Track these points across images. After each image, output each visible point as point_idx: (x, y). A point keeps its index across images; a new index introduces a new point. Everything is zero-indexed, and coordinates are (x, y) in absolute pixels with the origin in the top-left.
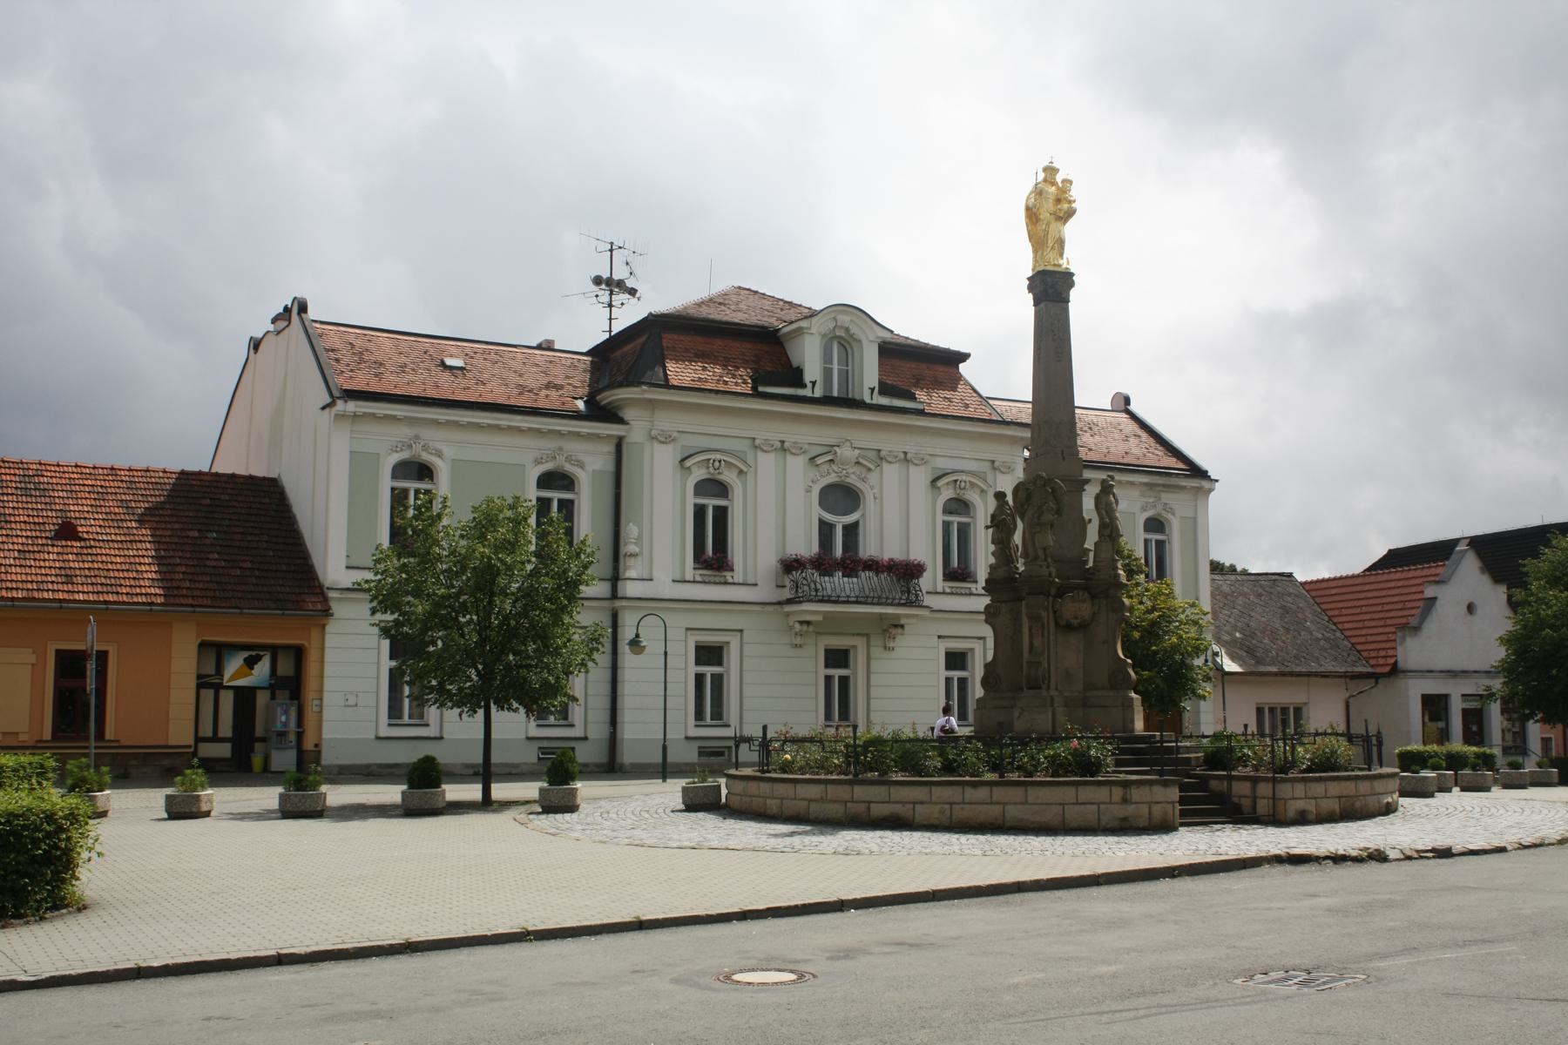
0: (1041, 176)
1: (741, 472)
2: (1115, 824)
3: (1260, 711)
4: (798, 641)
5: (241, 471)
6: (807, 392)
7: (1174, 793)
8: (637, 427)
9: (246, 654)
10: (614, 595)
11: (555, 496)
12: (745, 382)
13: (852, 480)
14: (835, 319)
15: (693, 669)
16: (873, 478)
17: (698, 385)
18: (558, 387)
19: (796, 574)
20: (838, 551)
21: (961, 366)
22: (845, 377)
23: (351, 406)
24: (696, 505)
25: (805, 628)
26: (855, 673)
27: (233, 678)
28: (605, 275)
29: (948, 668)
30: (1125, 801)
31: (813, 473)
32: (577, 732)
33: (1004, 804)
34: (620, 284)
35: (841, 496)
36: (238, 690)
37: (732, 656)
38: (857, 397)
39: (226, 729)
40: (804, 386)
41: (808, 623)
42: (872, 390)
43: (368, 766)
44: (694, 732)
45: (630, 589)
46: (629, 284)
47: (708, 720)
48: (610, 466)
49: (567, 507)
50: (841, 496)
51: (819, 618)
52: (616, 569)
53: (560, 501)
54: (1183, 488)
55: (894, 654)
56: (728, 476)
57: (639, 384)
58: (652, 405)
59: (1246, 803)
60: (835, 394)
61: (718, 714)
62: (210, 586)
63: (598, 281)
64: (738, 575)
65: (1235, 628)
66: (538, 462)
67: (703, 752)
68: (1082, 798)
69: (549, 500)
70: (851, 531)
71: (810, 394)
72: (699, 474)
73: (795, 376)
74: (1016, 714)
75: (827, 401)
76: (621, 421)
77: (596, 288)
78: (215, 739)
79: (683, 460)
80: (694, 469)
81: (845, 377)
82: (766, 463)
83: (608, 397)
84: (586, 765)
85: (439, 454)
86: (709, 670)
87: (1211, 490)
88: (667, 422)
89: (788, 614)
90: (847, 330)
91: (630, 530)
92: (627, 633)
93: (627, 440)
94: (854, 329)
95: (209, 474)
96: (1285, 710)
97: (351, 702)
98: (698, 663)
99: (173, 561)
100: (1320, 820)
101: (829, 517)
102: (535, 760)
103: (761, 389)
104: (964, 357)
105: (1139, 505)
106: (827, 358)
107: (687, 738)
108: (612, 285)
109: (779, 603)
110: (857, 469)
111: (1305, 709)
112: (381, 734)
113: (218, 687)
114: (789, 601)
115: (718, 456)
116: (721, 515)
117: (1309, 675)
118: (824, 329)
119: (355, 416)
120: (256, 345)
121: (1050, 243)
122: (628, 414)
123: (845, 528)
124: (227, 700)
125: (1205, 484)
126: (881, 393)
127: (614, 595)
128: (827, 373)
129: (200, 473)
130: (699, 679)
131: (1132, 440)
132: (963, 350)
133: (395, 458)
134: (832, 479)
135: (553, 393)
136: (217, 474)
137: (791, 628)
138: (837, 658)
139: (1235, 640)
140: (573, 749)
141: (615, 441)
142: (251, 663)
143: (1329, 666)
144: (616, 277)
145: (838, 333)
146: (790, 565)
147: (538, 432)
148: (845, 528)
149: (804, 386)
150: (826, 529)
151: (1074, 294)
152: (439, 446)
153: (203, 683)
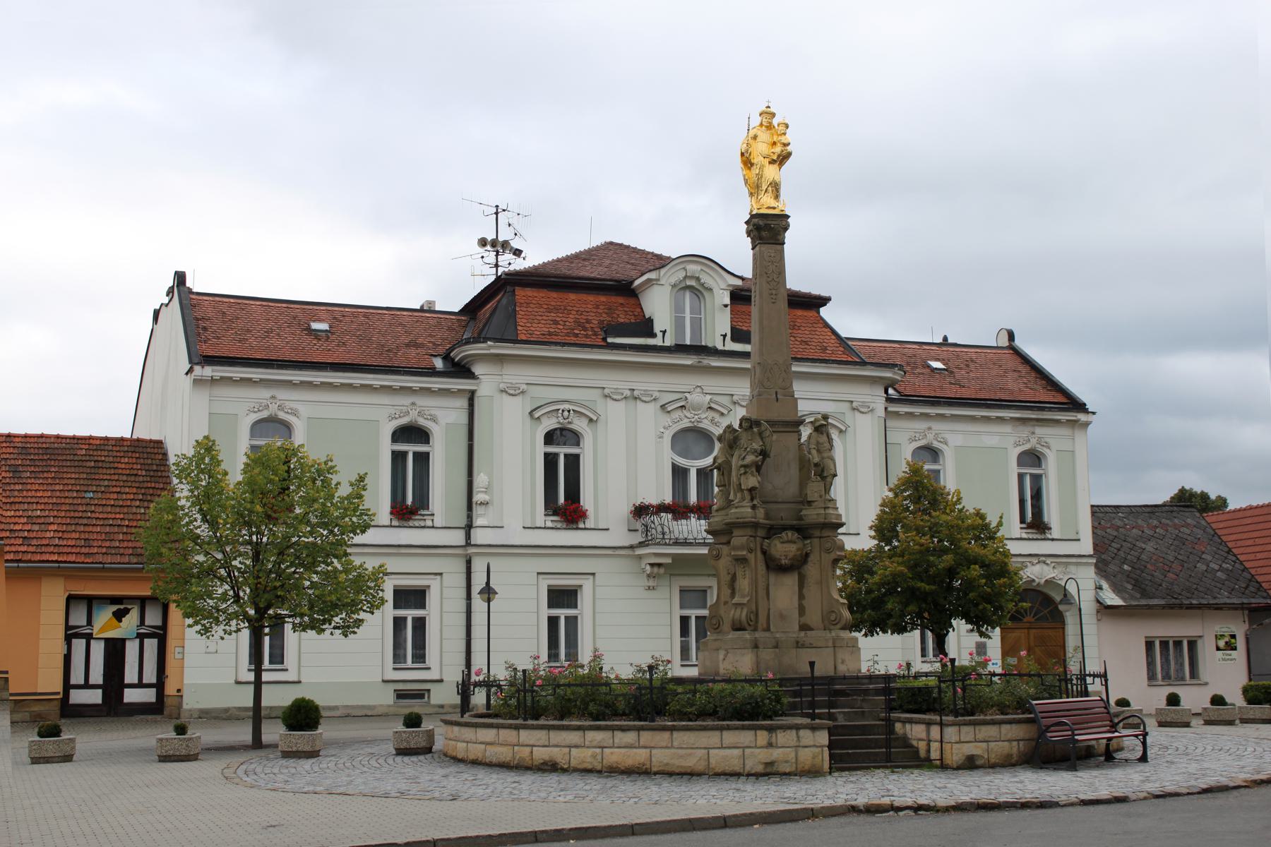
0: (756, 120)
1: (591, 420)
2: (760, 769)
3: (1149, 645)
5: (147, 437)
6: (657, 341)
7: (823, 738)
8: (487, 380)
9: (115, 608)
10: (468, 543)
11: (411, 448)
12: (595, 334)
17: (547, 339)
18: (417, 346)
19: (647, 519)
20: (693, 498)
21: (822, 310)
22: (697, 325)
23: (208, 371)
24: (546, 455)
25: (656, 569)
27: (102, 630)
28: (490, 236)
30: (770, 745)
31: (666, 420)
32: (433, 675)
33: (603, 748)
34: (505, 245)
36: (108, 641)
37: (585, 599)
38: (710, 345)
39: (97, 676)
40: (653, 335)
41: (659, 565)
42: (724, 336)
43: (227, 710)
45: (479, 536)
46: (515, 244)
48: (464, 419)
49: (423, 460)
51: (669, 561)
52: (470, 517)
53: (415, 454)
54: (1058, 422)
56: (579, 425)
57: (485, 340)
58: (500, 359)
59: (922, 746)
60: (688, 342)
61: (420, 656)
62: (78, 543)
63: (483, 243)
65: (1124, 561)
66: (392, 418)
67: (401, 695)
68: (726, 742)
69: (404, 454)
71: (660, 343)
72: (550, 424)
73: (646, 327)
74: (721, 657)
75: (680, 349)
76: (471, 375)
77: (481, 250)
78: (87, 685)
79: (531, 413)
81: (697, 325)
82: (614, 413)
83: (458, 354)
84: (442, 706)
85: (295, 413)
87: (1087, 424)
88: (516, 375)
89: (640, 557)
90: (698, 279)
91: (480, 479)
92: (479, 582)
93: (477, 394)
94: (705, 279)
95: (131, 440)
96: (1178, 644)
98: (550, 606)
99: (47, 520)
100: (992, 766)
101: (682, 462)
102: (392, 703)
103: (610, 340)
104: (823, 301)
105: (1012, 440)
106: (678, 308)
108: (498, 246)
109: (632, 547)
110: (711, 414)
111: (1200, 643)
112: (386, 678)
113: (89, 637)
114: (641, 545)
115: (567, 406)
116: (573, 463)
117: (1200, 607)
118: (673, 280)
119: (213, 381)
120: (156, 314)
121: (764, 188)
122: (478, 369)
123: (700, 472)
124: (98, 650)
125: (1082, 417)
126: (734, 339)
127: (468, 543)
128: (679, 323)
129: (122, 439)
130: (553, 622)
131: (1010, 375)
132: (824, 294)
134: (685, 424)
135: (413, 352)
136: (138, 440)
137: (644, 571)
139: (1122, 571)
140: (429, 691)
141: (468, 395)
142: (119, 616)
143: (1224, 598)
144: (501, 239)
145: (689, 283)
146: (640, 511)
149: (653, 335)
150: (679, 474)
151: (788, 235)
152: (293, 405)
153: (71, 635)
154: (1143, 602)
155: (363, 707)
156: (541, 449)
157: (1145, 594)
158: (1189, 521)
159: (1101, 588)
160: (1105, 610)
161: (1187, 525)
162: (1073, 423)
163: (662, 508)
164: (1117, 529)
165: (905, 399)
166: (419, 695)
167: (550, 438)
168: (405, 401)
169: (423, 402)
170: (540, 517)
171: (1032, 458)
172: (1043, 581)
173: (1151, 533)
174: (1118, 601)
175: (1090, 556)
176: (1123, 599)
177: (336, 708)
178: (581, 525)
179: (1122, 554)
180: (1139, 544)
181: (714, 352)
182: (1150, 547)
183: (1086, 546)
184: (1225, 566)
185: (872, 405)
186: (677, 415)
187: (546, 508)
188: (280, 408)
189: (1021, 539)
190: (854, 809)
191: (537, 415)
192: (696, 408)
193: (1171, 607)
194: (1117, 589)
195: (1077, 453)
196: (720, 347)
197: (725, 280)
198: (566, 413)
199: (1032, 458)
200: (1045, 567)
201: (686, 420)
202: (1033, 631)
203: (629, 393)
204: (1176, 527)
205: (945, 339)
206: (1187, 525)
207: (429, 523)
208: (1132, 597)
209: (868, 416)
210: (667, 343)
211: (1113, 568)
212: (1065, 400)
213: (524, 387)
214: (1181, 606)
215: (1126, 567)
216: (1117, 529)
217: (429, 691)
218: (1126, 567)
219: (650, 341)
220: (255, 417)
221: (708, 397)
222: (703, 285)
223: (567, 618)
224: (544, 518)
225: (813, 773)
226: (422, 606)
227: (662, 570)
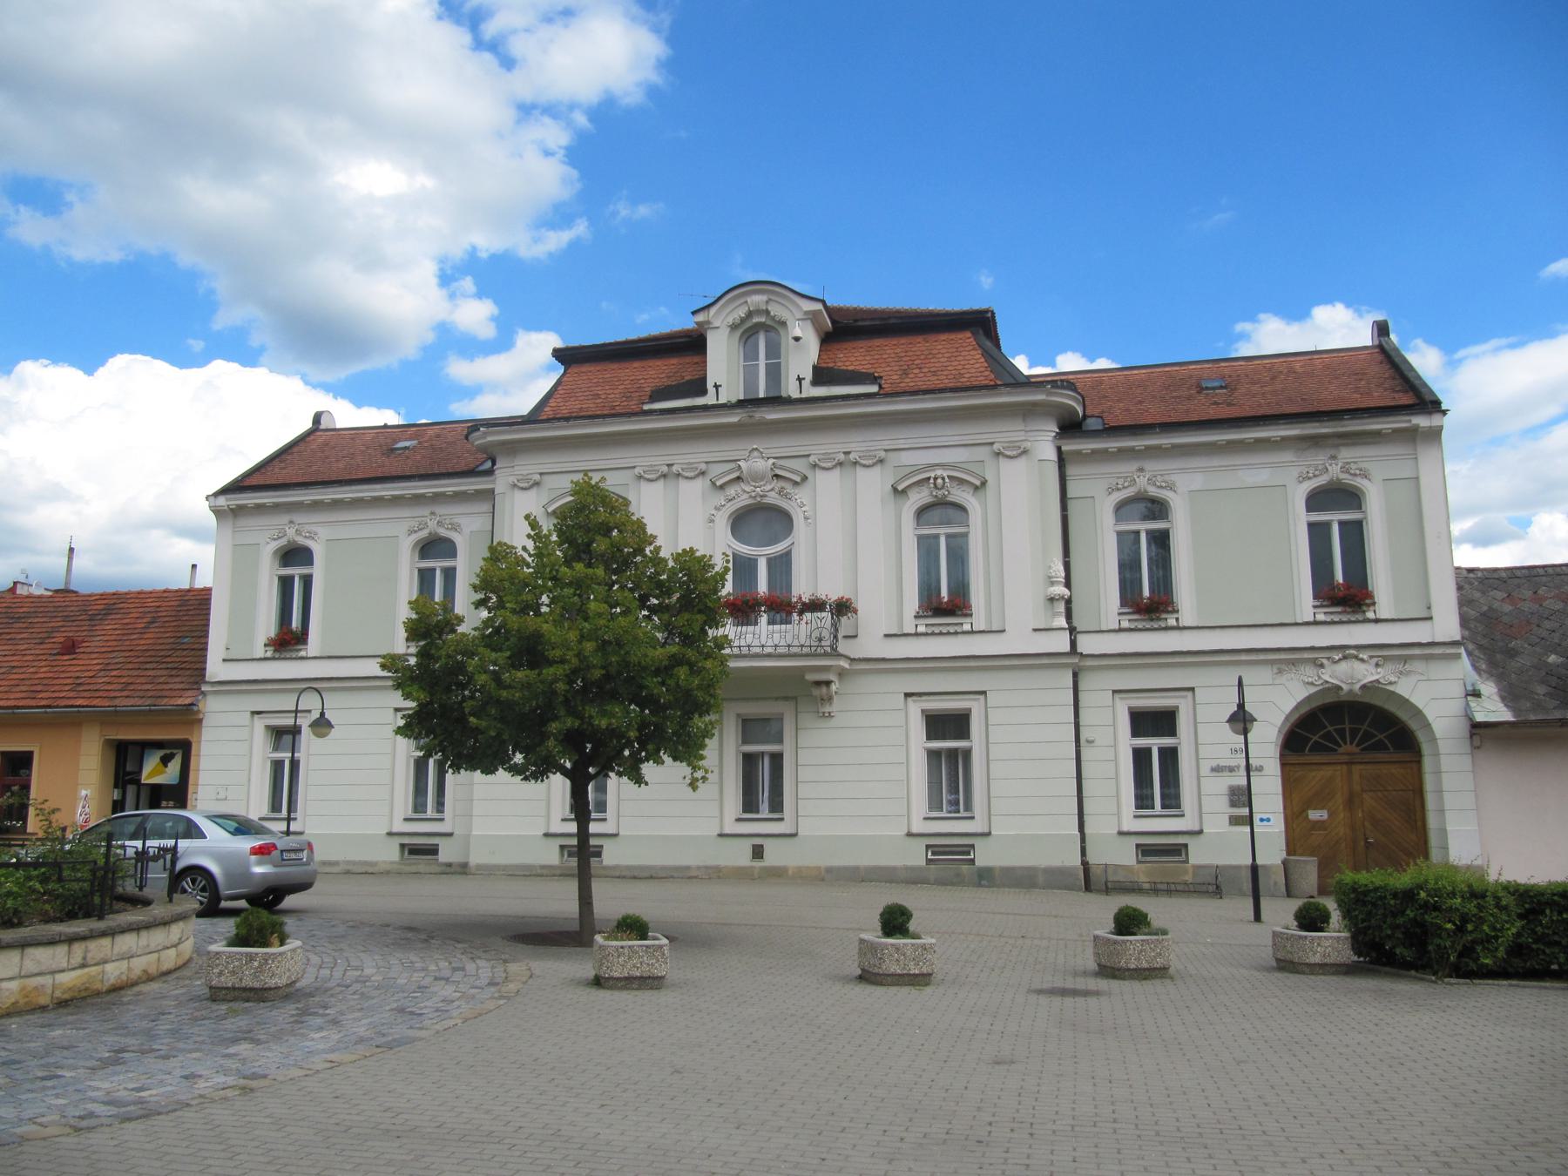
6: (709, 399)
9: (161, 753)
11: (1334, 518)
13: (773, 499)
15: (1126, 743)
16: (802, 495)
20: (762, 587)
27: (150, 776)
31: (720, 499)
37: (1183, 722)
44: (1130, 824)
47: (430, 812)
55: (833, 723)
60: (762, 395)
61: (1172, 800)
64: (979, 620)
66: (411, 532)
67: (1145, 851)
70: (781, 566)
72: (920, 497)
84: (450, 865)
86: (1155, 743)
94: (775, 310)
97: (222, 796)
105: (1295, 472)
107: (1121, 833)
115: (939, 472)
134: (744, 501)
138: (285, 735)
140: (1186, 846)
142: (165, 761)
145: (756, 320)
147: (418, 499)
148: (771, 562)
154: (1558, 715)
155: (366, 863)
159: (1476, 694)
160: (1479, 730)
162: (1412, 436)
166: (1178, 851)
167: (1316, 501)
168: (1129, 468)
169: (1152, 466)
171: (295, 555)
172: (1357, 687)
174: (1503, 714)
175: (1454, 644)
177: (336, 863)
178: (1370, 615)
181: (789, 401)
185: (1024, 445)
186: (731, 491)
187: (1124, 603)
188: (1345, 470)
189: (1316, 623)
191: (900, 488)
192: (756, 477)
194: (1510, 696)
195: (1423, 481)
196: (795, 394)
197: (798, 306)
198: (940, 481)
199: (295, 555)
200: (1356, 664)
201: (745, 496)
202: (1356, 769)
203: (665, 469)
207: (1172, 622)
209: (1021, 463)
210: (722, 400)
213: (883, 454)
217: (1186, 846)
218: (1552, 658)
219: (700, 401)
220: (1308, 486)
221: (771, 461)
222: (773, 318)
223: (1162, 751)
224: (914, 622)
226: (1172, 732)
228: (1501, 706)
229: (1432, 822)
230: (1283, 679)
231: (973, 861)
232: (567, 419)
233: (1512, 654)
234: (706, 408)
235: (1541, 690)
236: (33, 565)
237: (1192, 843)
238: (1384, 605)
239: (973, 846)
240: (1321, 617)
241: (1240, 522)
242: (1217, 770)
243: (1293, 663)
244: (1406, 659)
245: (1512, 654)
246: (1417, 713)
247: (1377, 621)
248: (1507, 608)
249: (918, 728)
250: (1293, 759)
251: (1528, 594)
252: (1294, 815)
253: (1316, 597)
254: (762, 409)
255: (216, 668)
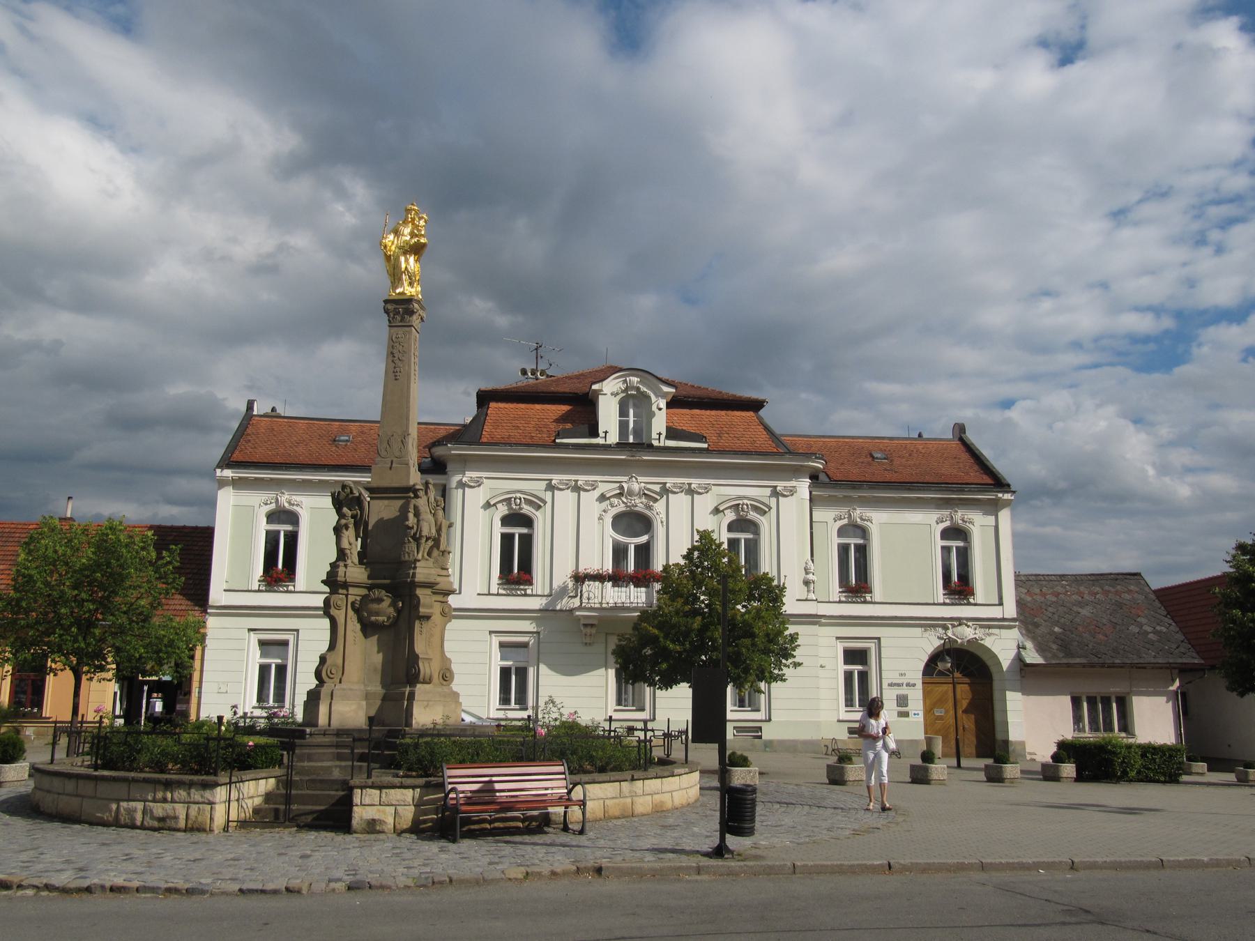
4: (588, 641)
6: (599, 441)
11: (517, 531)
13: (640, 508)
14: (625, 381)
16: (660, 506)
26: (870, 668)
29: (846, 663)
35: (634, 520)
44: (844, 716)
50: (634, 520)
65: (1057, 623)
80: (499, 506)
82: (565, 499)
98: (846, 663)
107: (839, 721)
115: (518, 495)
123: (637, 548)
126: (668, 437)
128: (623, 426)
133: (266, 509)
134: (622, 508)
148: (637, 548)
149: (596, 435)
150: (619, 553)
154: (1065, 661)
156: (498, 529)
157: (1069, 654)
158: (1132, 587)
159: (1024, 648)
161: (1130, 591)
163: (599, 578)
164: (1057, 595)
165: (834, 483)
170: (940, 595)
173: (1054, 599)
176: (1045, 658)
179: (1056, 617)
180: (1075, 609)
182: (1085, 612)
183: (1010, 610)
184: (1158, 628)
190: (263, 892)
193: (1092, 666)
194: (1041, 649)
204: (1117, 593)
205: (920, 435)
206: (1130, 591)
208: (1055, 656)
211: (1043, 630)
212: (990, 481)
214: (1103, 665)
215: (1057, 629)
216: (1057, 595)
218: (1057, 629)
225: (1202, 774)
227: (594, 631)
228: (1036, 655)
229: (998, 717)
230: (926, 634)
231: (760, 737)
232: (510, 445)
233: (1037, 625)
234: (597, 446)
235: (1054, 647)
236: (6, 517)
237: (765, 726)
238: (980, 596)
239: (760, 728)
240: (501, 591)
241: (906, 539)
242: (890, 685)
243: (934, 626)
244: (989, 627)
245: (1037, 625)
246: (995, 657)
247: (976, 605)
248: (1029, 599)
249: (255, 651)
250: (928, 679)
251: (1037, 591)
252: (928, 711)
253: (500, 578)
254: (636, 447)
255: (217, 594)
